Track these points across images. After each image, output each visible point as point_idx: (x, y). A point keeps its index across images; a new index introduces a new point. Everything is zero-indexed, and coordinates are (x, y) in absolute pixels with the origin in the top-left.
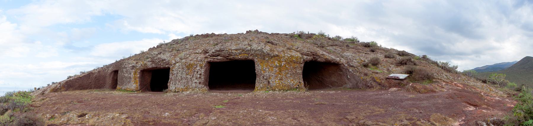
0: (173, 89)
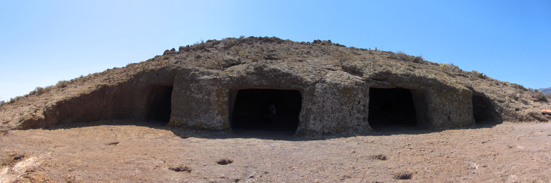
0: (319, 128)
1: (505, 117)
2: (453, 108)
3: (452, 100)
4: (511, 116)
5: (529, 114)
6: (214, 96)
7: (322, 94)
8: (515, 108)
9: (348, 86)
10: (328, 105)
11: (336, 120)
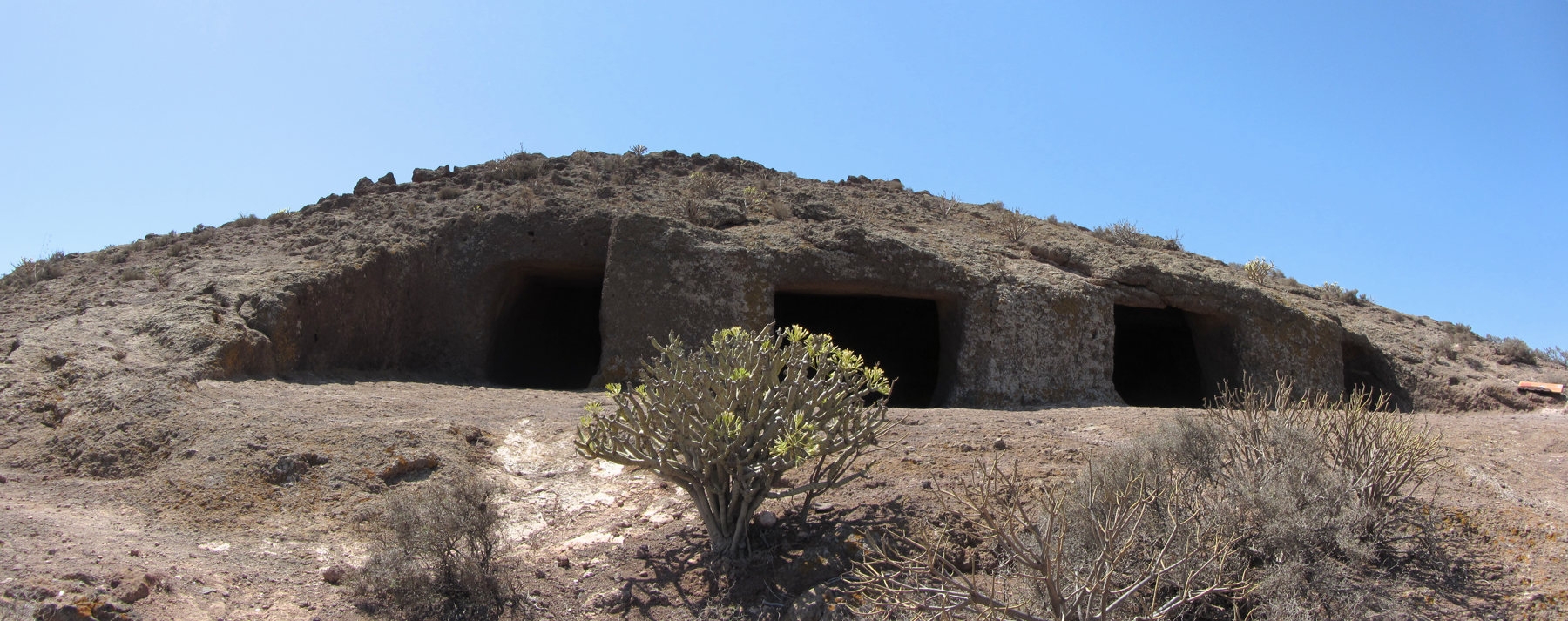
0: (1013, 389)
1: (1422, 400)
2: (1300, 362)
3: (1297, 344)
4: (1438, 398)
5: (1485, 391)
6: (742, 300)
7: (1015, 309)
8: (1448, 377)
9: (1069, 294)
10: (1029, 335)
11: (1047, 372)
